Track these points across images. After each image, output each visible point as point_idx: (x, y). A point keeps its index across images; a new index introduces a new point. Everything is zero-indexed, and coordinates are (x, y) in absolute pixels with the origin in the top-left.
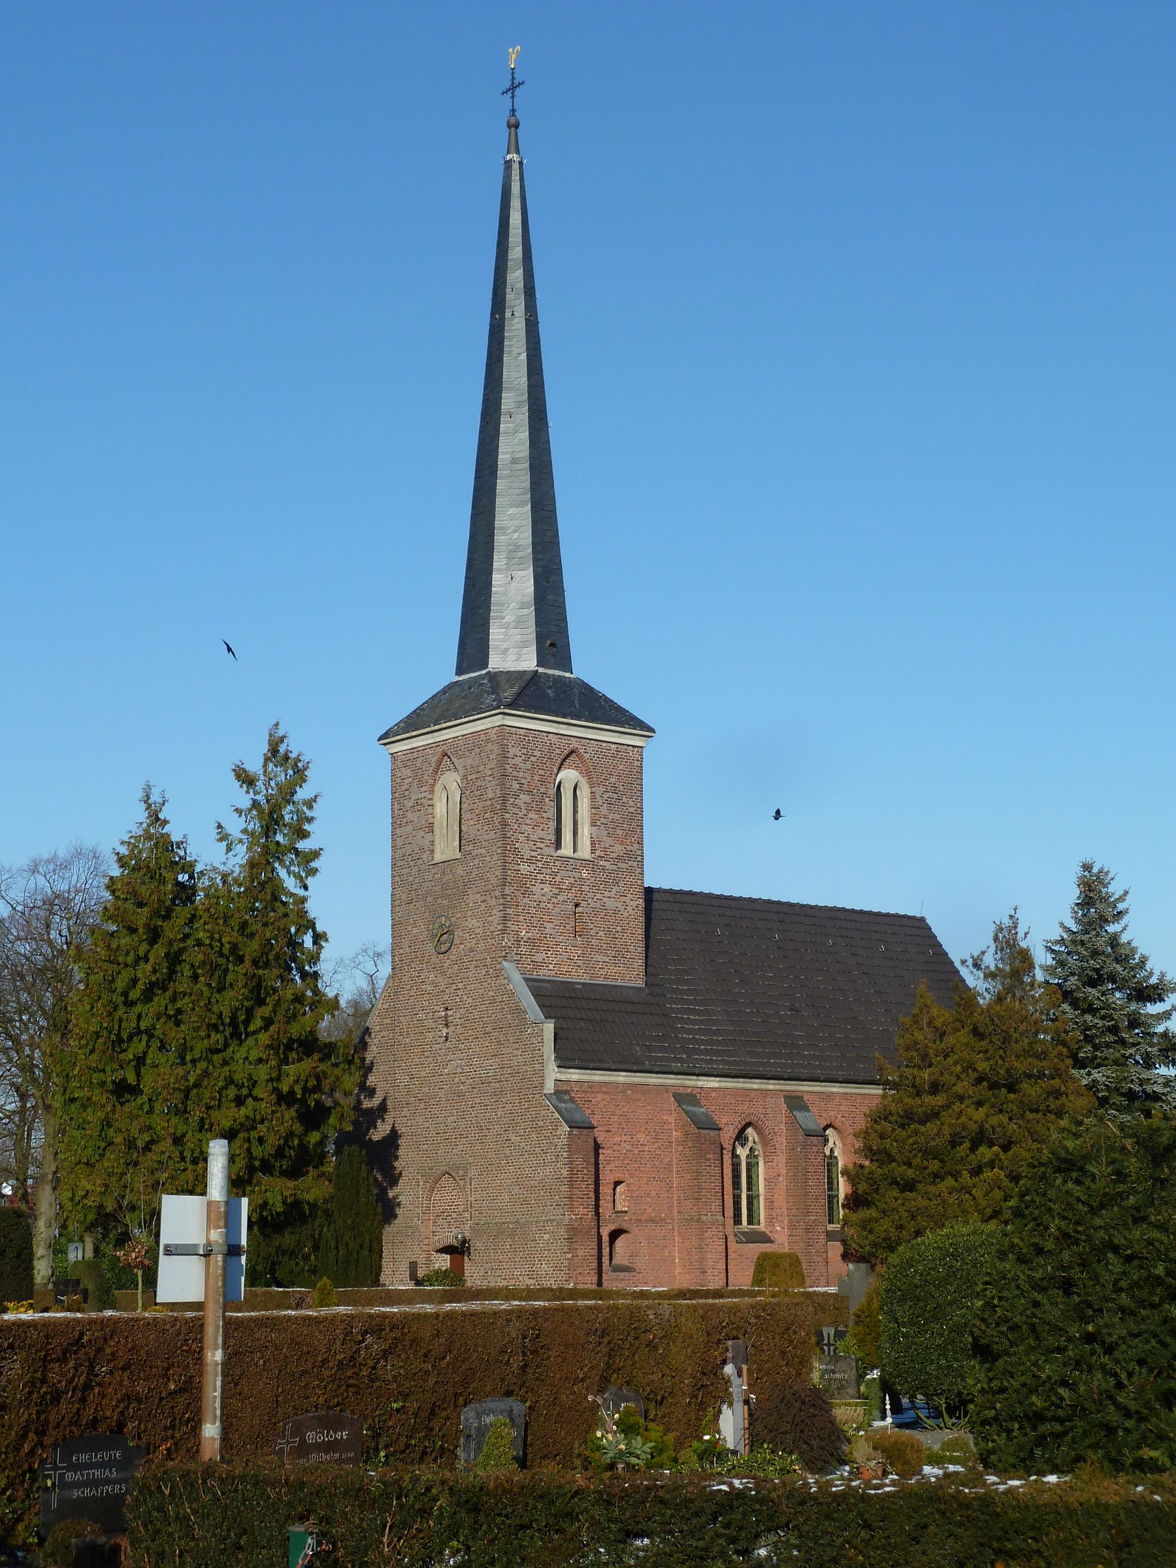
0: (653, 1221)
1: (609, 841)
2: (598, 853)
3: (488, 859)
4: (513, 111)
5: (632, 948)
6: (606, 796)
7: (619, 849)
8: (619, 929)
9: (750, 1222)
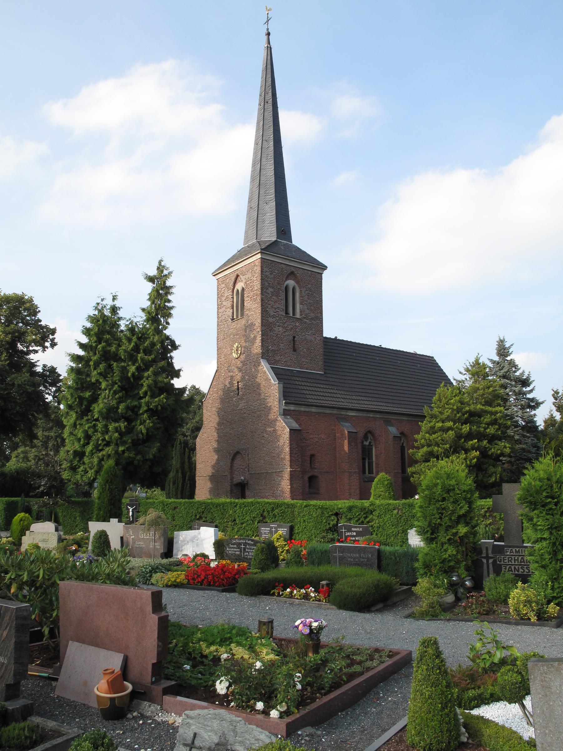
0: (328, 472)
1: (307, 311)
2: (303, 316)
3: (255, 316)
4: (268, 29)
5: (318, 357)
6: (307, 292)
7: (312, 315)
8: (313, 348)
9: (369, 473)
